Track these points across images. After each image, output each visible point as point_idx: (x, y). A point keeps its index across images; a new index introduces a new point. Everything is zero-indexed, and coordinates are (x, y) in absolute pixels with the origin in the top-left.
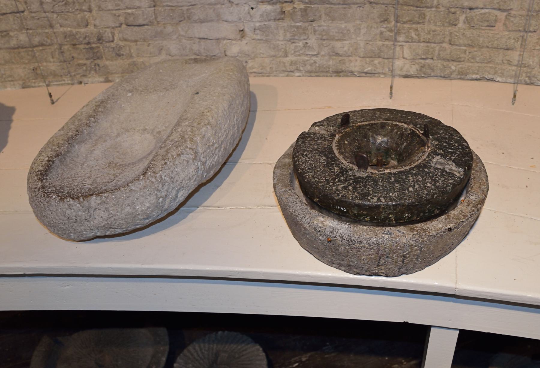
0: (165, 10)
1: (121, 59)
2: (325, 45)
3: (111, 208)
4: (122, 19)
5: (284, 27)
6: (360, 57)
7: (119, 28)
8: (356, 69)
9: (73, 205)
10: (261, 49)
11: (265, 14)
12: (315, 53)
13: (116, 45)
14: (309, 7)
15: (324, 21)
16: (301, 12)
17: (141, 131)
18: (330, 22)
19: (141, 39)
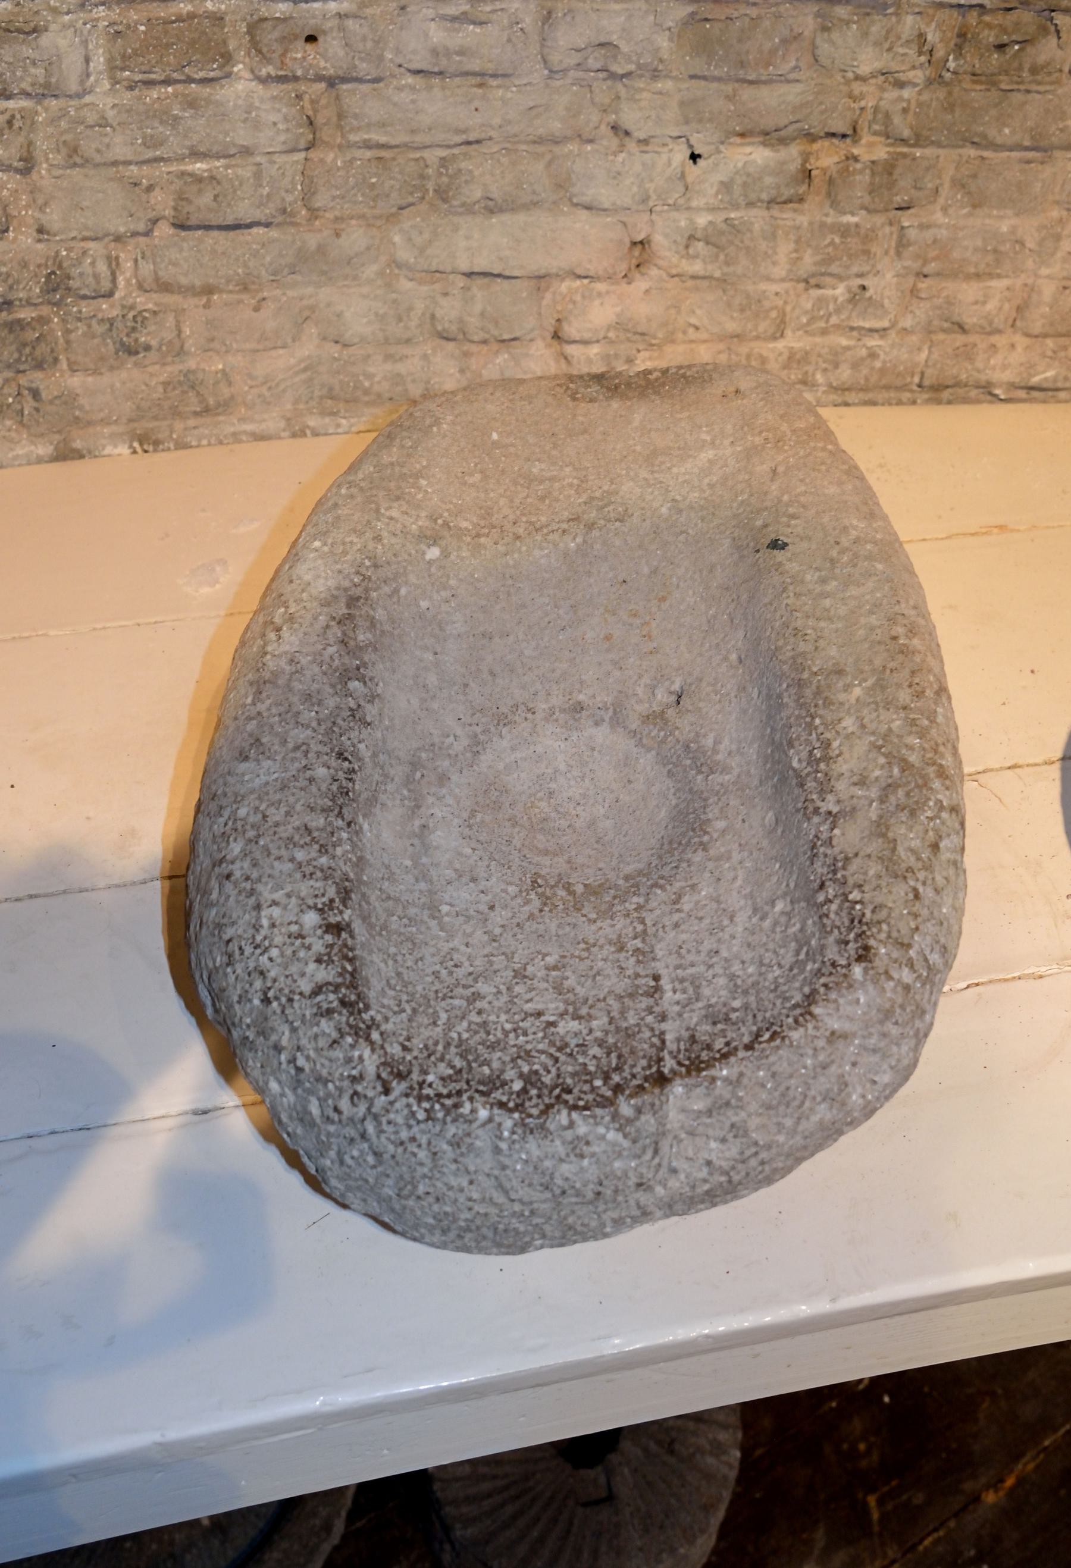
0: (352, 161)
1: (136, 364)
2: (923, 295)
3: (754, 1122)
4: (162, 201)
5: (798, 228)
6: (1027, 335)
7: (142, 240)
8: (1007, 376)
9: (590, 1138)
10: (694, 312)
11: (739, 180)
12: (886, 324)
13: (123, 307)
14: (905, 156)
15: (945, 210)
16: (873, 174)
17: (562, 717)
18: (965, 211)
19: (228, 281)
